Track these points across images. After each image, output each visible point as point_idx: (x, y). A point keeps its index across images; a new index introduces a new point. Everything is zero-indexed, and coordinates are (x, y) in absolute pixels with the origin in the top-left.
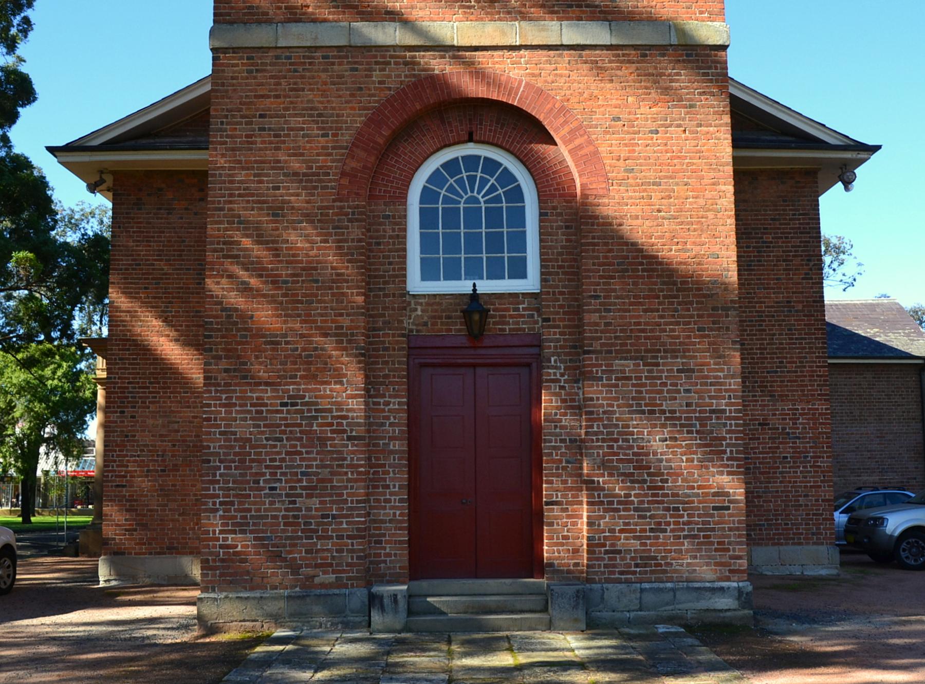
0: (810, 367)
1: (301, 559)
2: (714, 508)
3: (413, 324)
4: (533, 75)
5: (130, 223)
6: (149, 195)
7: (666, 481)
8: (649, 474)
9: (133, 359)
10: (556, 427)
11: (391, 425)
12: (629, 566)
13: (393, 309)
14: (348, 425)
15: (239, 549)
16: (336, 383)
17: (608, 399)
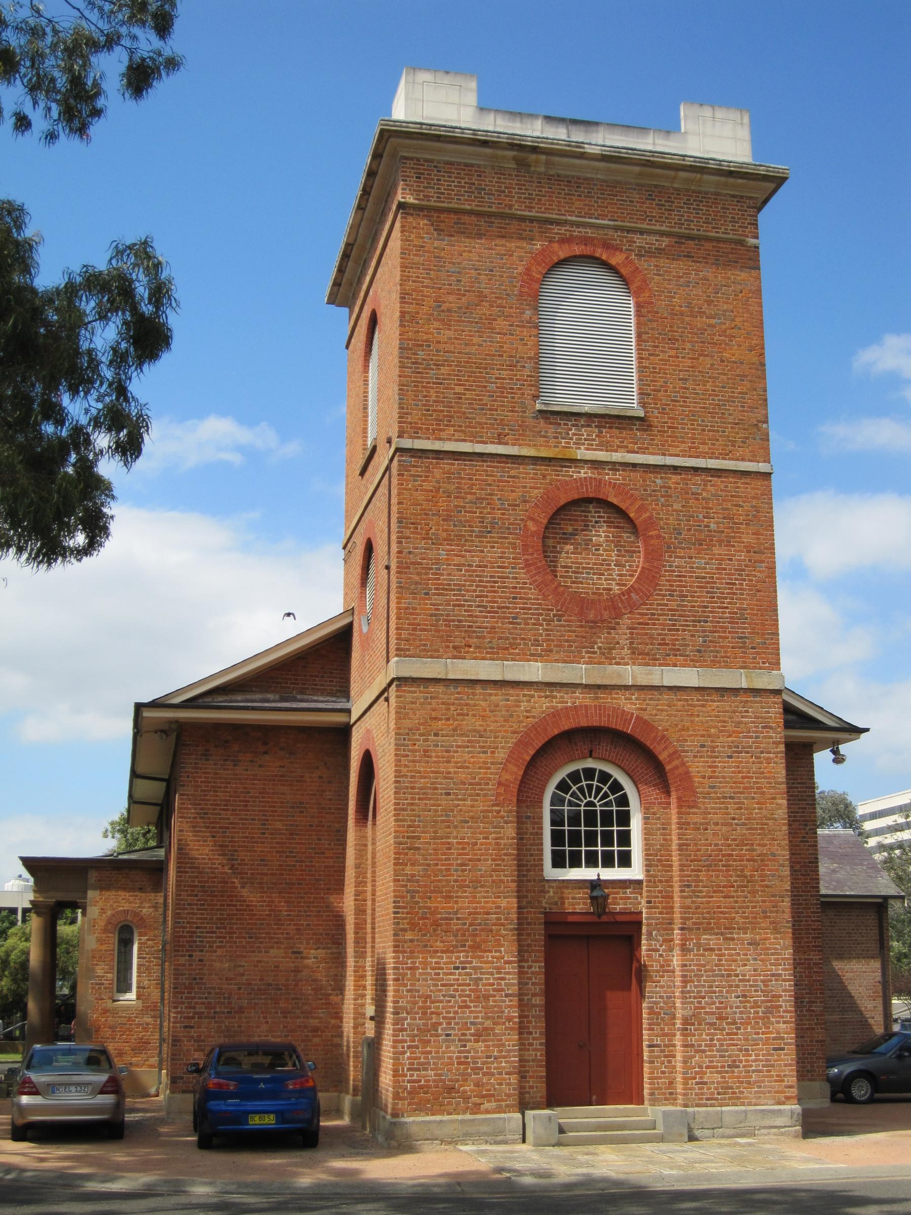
0: (806, 921)
1: (472, 1091)
2: (774, 1049)
3: (546, 903)
4: (641, 709)
5: (198, 773)
6: (216, 746)
7: (739, 1029)
8: (727, 1024)
9: (201, 905)
10: (656, 986)
11: (533, 984)
12: (713, 1093)
13: (534, 892)
14: (506, 985)
15: (422, 1083)
16: (496, 951)
17: (698, 965)
